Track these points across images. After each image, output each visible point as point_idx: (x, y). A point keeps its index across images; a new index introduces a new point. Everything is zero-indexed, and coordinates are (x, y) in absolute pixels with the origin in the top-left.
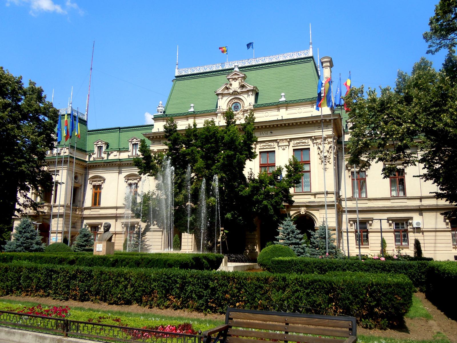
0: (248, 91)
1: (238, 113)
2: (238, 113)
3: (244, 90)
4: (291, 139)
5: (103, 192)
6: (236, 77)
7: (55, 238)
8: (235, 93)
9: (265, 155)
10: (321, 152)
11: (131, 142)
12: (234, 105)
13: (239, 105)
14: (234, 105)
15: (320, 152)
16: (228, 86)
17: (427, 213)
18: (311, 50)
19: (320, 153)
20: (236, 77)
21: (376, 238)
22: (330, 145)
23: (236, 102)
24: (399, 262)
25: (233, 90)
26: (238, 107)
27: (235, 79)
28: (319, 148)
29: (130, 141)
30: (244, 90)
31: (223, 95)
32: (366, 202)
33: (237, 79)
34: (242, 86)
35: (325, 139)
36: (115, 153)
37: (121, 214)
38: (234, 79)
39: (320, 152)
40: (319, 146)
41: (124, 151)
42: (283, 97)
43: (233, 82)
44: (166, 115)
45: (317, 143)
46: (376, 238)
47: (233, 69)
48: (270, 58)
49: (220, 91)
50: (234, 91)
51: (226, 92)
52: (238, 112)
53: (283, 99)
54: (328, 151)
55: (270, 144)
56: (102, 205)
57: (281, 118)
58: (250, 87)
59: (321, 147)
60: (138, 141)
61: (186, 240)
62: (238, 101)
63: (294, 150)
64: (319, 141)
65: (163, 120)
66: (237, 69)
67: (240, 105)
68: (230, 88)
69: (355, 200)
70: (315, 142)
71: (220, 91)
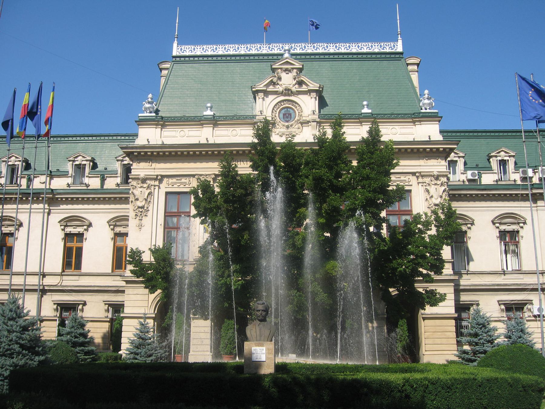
0: (310, 92)
1: (291, 126)
2: (291, 126)
3: (304, 88)
4: (160, 179)
5: (87, 247)
6: (289, 67)
7: (539, 330)
8: (288, 92)
9: (174, 198)
10: (432, 197)
11: (74, 161)
12: (283, 111)
13: (291, 111)
14: (283, 111)
15: (428, 198)
16: (275, 80)
17: (485, 297)
18: (400, 43)
19: (429, 199)
20: (289, 67)
21: (202, 329)
22: (443, 188)
23: (287, 108)
24: (136, 361)
25: (284, 86)
26: (290, 114)
27: (286, 70)
28: (428, 191)
29: (71, 159)
30: (304, 88)
31: (266, 93)
32: (521, 276)
33: (290, 71)
34: (301, 83)
35: (437, 178)
36: (43, 178)
37: (52, 286)
38: (286, 70)
39: (428, 198)
40: (428, 187)
41: (59, 176)
42: (209, 109)
43: (283, 75)
44: (162, 118)
45: (423, 183)
46: (202, 329)
47: (282, 55)
48: (203, 49)
49: (262, 86)
50: (286, 90)
51: (271, 89)
52: (291, 123)
53: (209, 113)
54: (146, 200)
55: (183, 180)
56: (85, 267)
57: (206, 142)
58: (314, 86)
59: (432, 189)
60: (87, 160)
61: (203, 336)
62: (290, 106)
63: (167, 193)
64: (427, 180)
65: (157, 125)
66: (286, 55)
67: (295, 112)
68: (278, 84)
69: (536, 273)
70: (420, 180)
71: (261, 86)
